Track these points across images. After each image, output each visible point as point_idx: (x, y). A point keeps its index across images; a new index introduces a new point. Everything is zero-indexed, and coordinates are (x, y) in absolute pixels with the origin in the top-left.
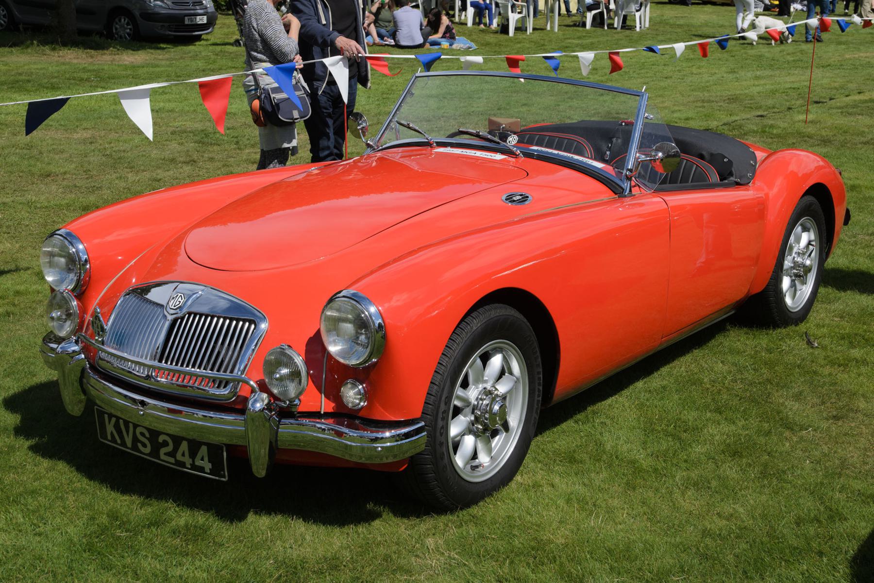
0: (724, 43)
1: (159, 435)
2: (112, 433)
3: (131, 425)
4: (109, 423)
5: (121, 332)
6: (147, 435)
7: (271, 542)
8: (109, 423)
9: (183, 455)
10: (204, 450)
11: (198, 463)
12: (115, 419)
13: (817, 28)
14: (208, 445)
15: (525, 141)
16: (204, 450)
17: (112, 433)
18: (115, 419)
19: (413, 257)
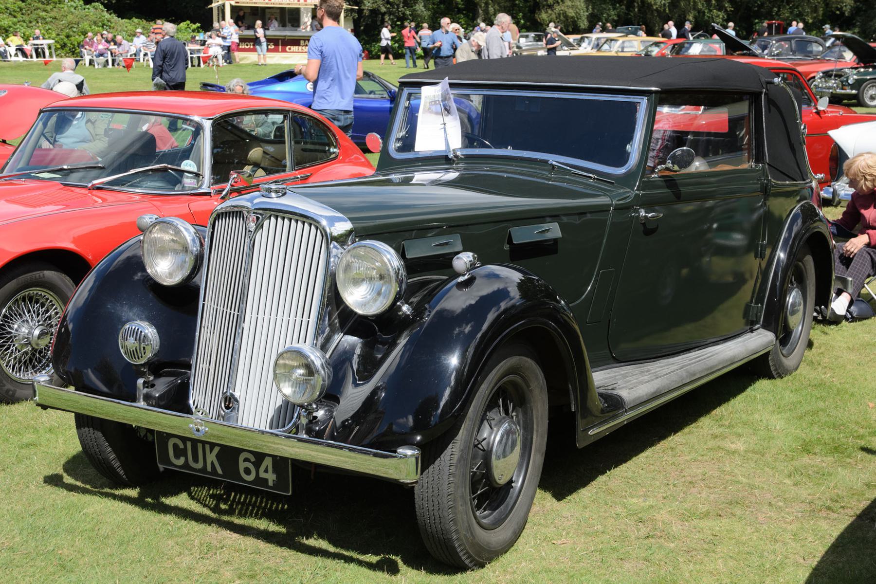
0: (337, 81)
1: (240, 454)
2: (212, 463)
3: (200, 446)
4: (211, 452)
5: (226, 220)
6: (253, 459)
7: (783, 517)
8: (211, 452)
9: (266, 471)
10: (268, 462)
11: (262, 475)
12: (209, 446)
13: (269, 19)
14: (274, 457)
15: (280, 41)
16: (268, 462)
17: (212, 463)
18: (209, 446)
19: (481, 410)
